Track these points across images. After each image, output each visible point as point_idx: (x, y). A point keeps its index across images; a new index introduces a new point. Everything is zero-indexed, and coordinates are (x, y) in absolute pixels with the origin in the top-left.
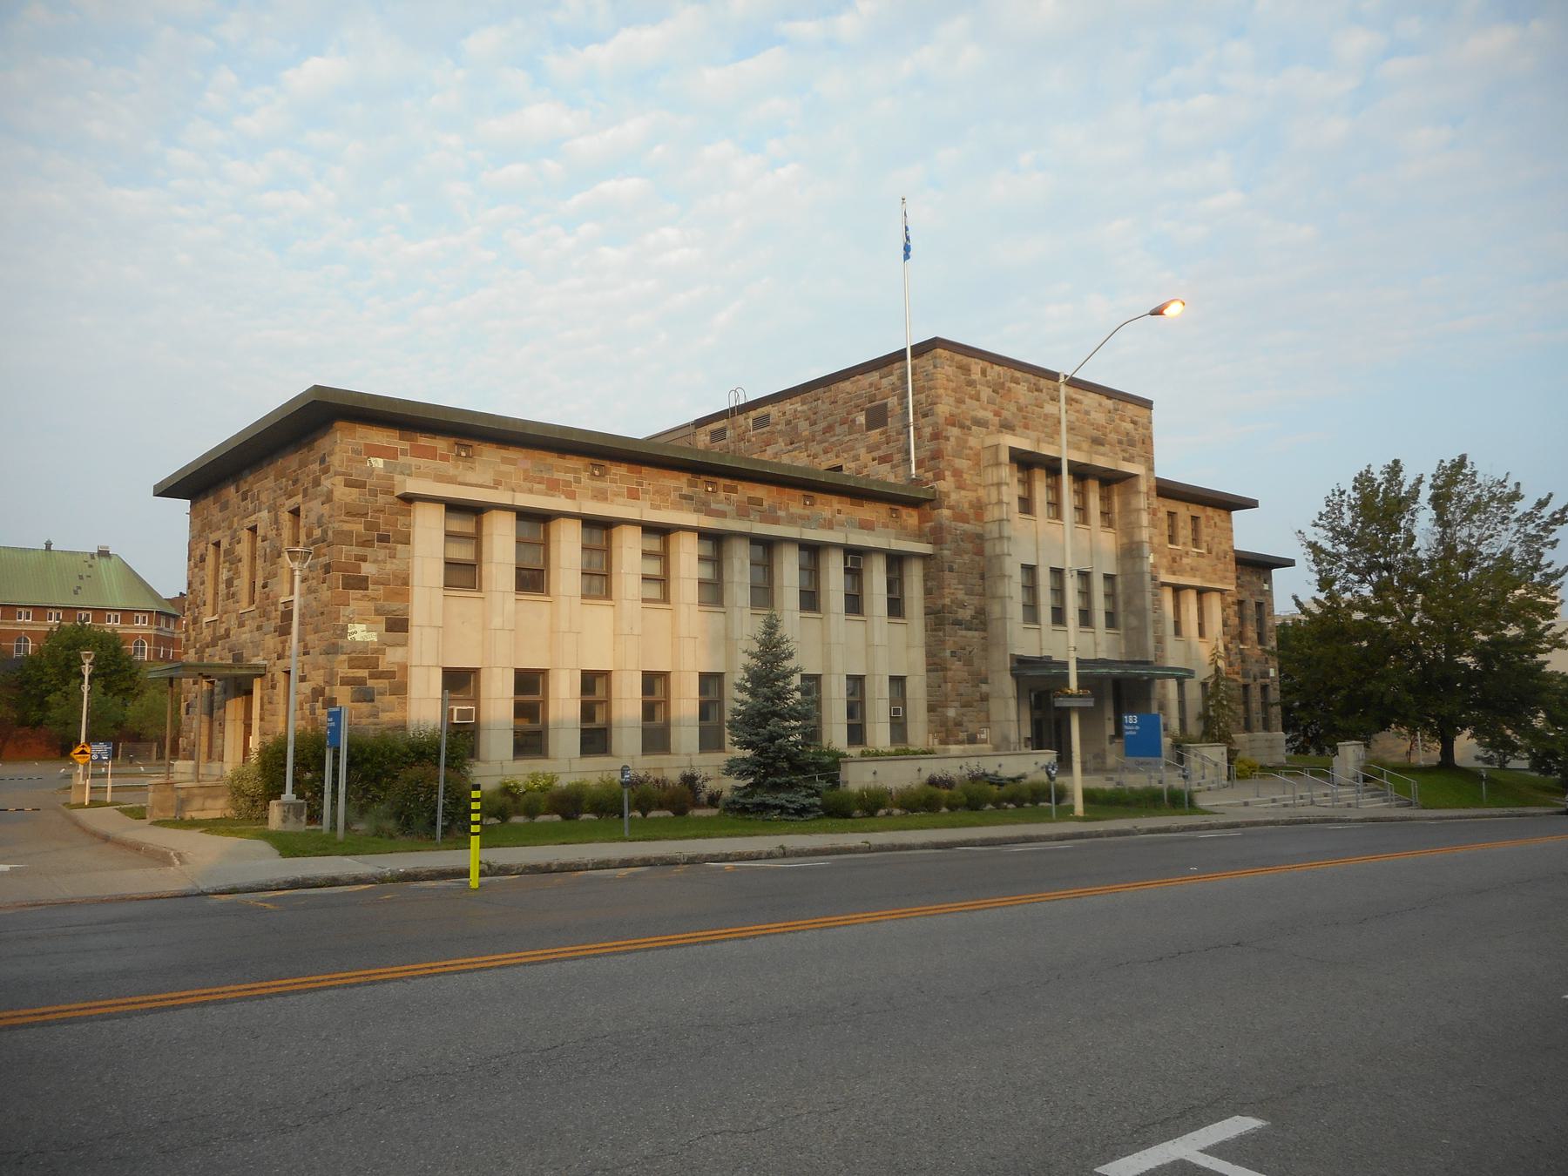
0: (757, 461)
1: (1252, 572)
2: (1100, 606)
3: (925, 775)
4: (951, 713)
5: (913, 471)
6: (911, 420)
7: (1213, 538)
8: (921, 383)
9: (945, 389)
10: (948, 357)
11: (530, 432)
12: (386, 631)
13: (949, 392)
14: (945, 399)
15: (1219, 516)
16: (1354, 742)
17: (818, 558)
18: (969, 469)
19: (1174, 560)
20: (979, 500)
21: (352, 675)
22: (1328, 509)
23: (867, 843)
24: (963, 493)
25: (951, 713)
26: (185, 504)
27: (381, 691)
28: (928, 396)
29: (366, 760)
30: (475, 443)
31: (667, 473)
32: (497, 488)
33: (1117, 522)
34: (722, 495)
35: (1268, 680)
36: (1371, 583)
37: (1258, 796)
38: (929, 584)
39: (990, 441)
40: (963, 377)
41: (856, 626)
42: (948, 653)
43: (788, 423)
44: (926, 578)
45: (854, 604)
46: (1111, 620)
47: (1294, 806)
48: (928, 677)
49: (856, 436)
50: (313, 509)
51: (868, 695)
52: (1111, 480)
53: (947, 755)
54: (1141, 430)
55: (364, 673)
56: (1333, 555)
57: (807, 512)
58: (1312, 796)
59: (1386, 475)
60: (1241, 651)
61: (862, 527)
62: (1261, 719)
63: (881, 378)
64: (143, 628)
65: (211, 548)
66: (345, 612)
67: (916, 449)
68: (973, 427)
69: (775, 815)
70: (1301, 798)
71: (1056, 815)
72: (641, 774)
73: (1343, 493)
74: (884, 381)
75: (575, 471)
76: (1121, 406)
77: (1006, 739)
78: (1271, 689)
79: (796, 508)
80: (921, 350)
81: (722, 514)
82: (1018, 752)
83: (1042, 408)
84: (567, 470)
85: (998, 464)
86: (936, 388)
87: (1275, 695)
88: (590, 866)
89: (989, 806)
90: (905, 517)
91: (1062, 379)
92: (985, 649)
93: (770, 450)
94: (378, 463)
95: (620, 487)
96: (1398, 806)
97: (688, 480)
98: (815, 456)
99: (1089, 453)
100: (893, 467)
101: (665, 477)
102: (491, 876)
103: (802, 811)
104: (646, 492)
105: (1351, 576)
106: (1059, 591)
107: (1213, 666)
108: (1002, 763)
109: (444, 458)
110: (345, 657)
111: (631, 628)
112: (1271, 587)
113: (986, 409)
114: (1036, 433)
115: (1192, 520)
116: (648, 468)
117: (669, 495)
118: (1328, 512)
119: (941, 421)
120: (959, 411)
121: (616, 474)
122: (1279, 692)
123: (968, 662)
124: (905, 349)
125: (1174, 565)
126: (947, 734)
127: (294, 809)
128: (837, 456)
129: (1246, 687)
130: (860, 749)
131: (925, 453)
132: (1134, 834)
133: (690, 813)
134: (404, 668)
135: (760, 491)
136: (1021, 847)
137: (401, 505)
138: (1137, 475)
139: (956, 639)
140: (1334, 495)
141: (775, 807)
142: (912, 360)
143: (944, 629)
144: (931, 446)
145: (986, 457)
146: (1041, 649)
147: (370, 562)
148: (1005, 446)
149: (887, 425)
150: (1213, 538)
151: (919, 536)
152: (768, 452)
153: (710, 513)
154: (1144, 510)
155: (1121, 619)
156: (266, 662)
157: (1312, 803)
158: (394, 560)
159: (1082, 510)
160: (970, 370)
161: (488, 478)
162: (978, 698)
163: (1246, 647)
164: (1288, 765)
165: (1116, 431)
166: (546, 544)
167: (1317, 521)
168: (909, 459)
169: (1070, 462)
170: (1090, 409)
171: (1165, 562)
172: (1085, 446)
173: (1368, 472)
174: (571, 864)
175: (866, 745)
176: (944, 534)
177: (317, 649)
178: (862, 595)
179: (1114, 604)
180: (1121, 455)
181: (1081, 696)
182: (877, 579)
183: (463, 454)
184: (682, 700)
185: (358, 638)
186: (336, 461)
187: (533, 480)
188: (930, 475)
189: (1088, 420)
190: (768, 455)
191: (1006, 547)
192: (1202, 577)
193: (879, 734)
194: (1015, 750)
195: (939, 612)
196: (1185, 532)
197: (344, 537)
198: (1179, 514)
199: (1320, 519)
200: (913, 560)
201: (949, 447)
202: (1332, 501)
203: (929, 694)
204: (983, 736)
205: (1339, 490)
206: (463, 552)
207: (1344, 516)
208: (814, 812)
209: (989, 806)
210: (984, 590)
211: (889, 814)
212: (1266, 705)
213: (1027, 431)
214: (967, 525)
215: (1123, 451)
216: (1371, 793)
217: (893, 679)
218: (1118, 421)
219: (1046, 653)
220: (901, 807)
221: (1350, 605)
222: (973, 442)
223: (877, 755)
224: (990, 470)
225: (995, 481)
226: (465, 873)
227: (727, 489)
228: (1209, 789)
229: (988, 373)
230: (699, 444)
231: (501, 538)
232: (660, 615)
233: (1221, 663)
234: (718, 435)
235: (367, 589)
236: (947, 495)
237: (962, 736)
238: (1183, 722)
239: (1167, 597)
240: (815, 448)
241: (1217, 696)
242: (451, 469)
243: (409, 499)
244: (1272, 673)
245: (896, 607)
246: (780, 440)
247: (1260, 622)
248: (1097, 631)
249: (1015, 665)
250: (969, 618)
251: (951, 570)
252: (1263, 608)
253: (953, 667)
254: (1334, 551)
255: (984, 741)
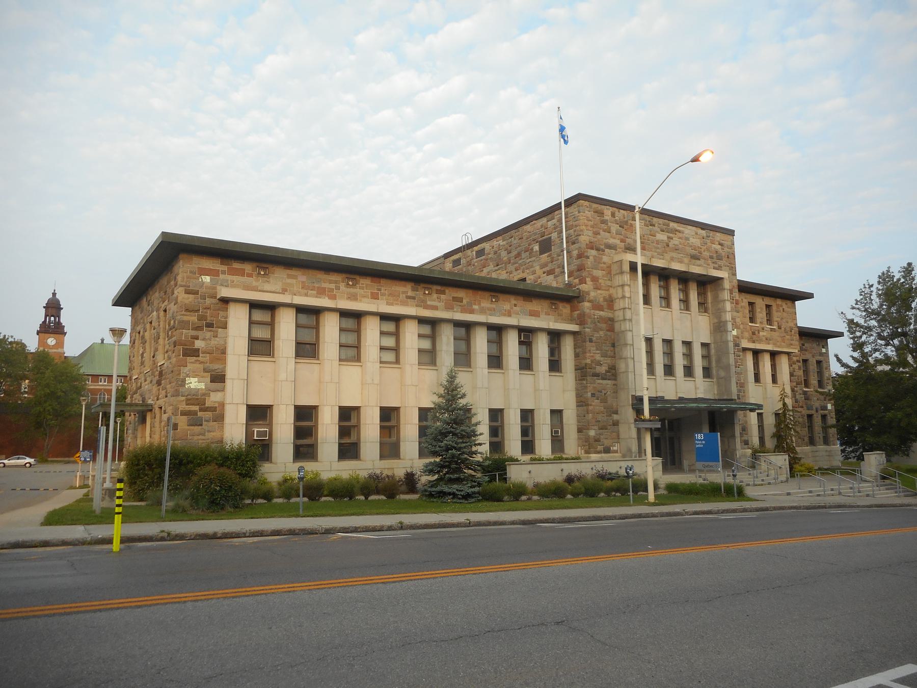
0: (479, 277)
1: (813, 341)
2: (698, 364)
3: (565, 474)
4: (592, 433)
5: (566, 279)
6: (565, 247)
7: (782, 319)
8: (571, 223)
9: (586, 226)
10: (588, 205)
11: (301, 258)
12: (211, 382)
13: (589, 228)
14: (586, 232)
15: (786, 304)
16: (878, 452)
17: (502, 335)
18: (603, 276)
19: (754, 333)
20: (610, 296)
21: (189, 409)
22: (862, 297)
23: (468, 520)
24: (599, 292)
25: (592, 433)
26: (128, 310)
27: (207, 419)
28: (575, 231)
29: (191, 462)
30: (270, 266)
31: (398, 283)
32: (284, 294)
33: (710, 309)
34: (435, 296)
35: (826, 412)
36: (894, 346)
37: (799, 489)
38: (577, 350)
39: (617, 258)
40: (599, 218)
41: (527, 377)
42: (589, 394)
43: (495, 253)
44: (576, 347)
45: (526, 363)
46: (707, 372)
47: (824, 495)
48: (578, 410)
49: (534, 258)
50: (172, 308)
51: (536, 422)
52: (706, 283)
53: (590, 460)
54: (726, 249)
55: (196, 408)
56: (866, 328)
57: (494, 306)
58: (839, 489)
59: (902, 273)
60: (805, 393)
61: (531, 315)
62: (821, 437)
63: (548, 221)
64: (105, 385)
65: (137, 334)
66: (185, 370)
67: (568, 265)
68: (606, 250)
69: (449, 499)
70: (832, 490)
71: (633, 501)
72: (378, 472)
73: (872, 286)
74: (550, 223)
75: (336, 282)
76: (711, 235)
77: (630, 450)
78: (829, 417)
79: (486, 304)
80: (570, 202)
81: (435, 308)
82: (638, 458)
83: (655, 236)
84: (331, 282)
85: (622, 273)
86: (580, 226)
87: (832, 420)
88: (247, 535)
89: (602, 494)
90: (561, 308)
91: (637, 209)
92: (616, 392)
93: (485, 270)
94: (207, 279)
95: (366, 292)
96: (906, 496)
97: (412, 286)
98: (511, 273)
99: (688, 265)
100: (555, 277)
101: (396, 285)
102: (169, 541)
103: (467, 497)
104: (383, 295)
105: (879, 341)
106: (689, 355)
107: (782, 402)
108: (564, 468)
109: (250, 275)
110: (183, 398)
111: (373, 380)
112: (827, 350)
113: (614, 238)
114: (651, 253)
115: (766, 307)
116: (384, 280)
117: (399, 296)
118: (862, 299)
119: (584, 246)
120: (596, 239)
121: (363, 284)
122: (835, 419)
123: (604, 401)
124: (561, 202)
125: (754, 335)
126: (589, 447)
127: (109, 492)
128: (523, 272)
129: (810, 417)
130: (529, 457)
131: (574, 267)
132: (682, 515)
133: (398, 497)
134: (222, 405)
135: (461, 293)
136: (834, 510)
137: (220, 305)
138: (723, 278)
139: (595, 385)
140: (865, 288)
141: (450, 494)
142: (565, 209)
143: (587, 380)
144: (578, 262)
145: (615, 268)
146: (677, 392)
147: (200, 340)
148: (626, 261)
149: (551, 250)
150: (782, 319)
151: (571, 320)
152: (484, 272)
153: (427, 307)
154: (728, 300)
155: (714, 372)
156: (152, 402)
157: (840, 493)
158: (216, 339)
159: (685, 302)
160: (603, 214)
161: (278, 287)
162: (611, 424)
163: (809, 390)
164: (842, 467)
165: (708, 250)
166: (317, 328)
167: (854, 306)
168: (564, 272)
169: (643, 265)
170: (689, 236)
171: (746, 335)
172: (686, 260)
173: (888, 271)
174: (232, 533)
175: (535, 454)
176: (586, 318)
177: (170, 393)
178: (532, 358)
179: (710, 362)
180: (712, 265)
181: (650, 421)
182: (512, 346)
183: (262, 273)
184: (407, 425)
185: (192, 386)
186: (179, 278)
187: (308, 288)
188: (577, 281)
189: (688, 243)
190: (484, 273)
191: (627, 325)
192: (774, 344)
193: (544, 447)
194: (635, 457)
195: (583, 368)
196: (761, 315)
197: (184, 325)
198: (756, 303)
199: (856, 304)
200: (539, 334)
201: (589, 262)
202: (864, 292)
203: (578, 421)
204: (615, 448)
205: (869, 284)
206: (261, 333)
207: (873, 302)
208: (475, 497)
209: (602, 494)
210: (615, 354)
211: (529, 499)
212: (825, 428)
213: (644, 251)
214: (602, 312)
215: (713, 263)
216: (886, 487)
217: (553, 412)
218: (709, 244)
219: (659, 394)
220: (539, 495)
221: (878, 362)
222: (605, 259)
223: (540, 460)
224: (617, 277)
225: (621, 284)
226: (109, 541)
227: (438, 292)
228: (769, 484)
229: (616, 215)
230: (446, 268)
231: (286, 325)
232: (392, 373)
233: (789, 402)
234: (457, 263)
235: (199, 356)
236: (588, 293)
237: (600, 448)
238: (762, 439)
239: (749, 359)
240: (511, 268)
241: (785, 422)
242: (254, 282)
243: (226, 301)
244: (829, 406)
245: (555, 365)
246: (491, 263)
247: (820, 373)
248: (697, 380)
249: (635, 402)
250: (604, 372)
251: (591, 341)
252: (822, 365)
253: (593, 404)
254: (866, 325)
255: (616, 452)
